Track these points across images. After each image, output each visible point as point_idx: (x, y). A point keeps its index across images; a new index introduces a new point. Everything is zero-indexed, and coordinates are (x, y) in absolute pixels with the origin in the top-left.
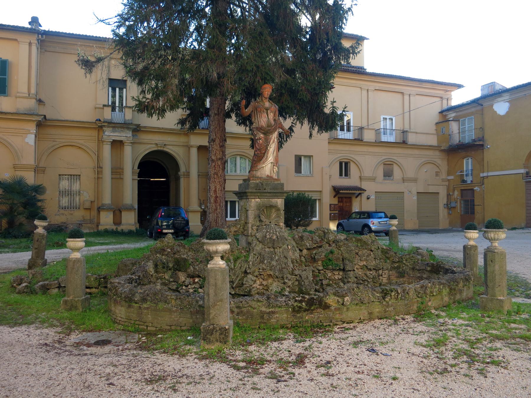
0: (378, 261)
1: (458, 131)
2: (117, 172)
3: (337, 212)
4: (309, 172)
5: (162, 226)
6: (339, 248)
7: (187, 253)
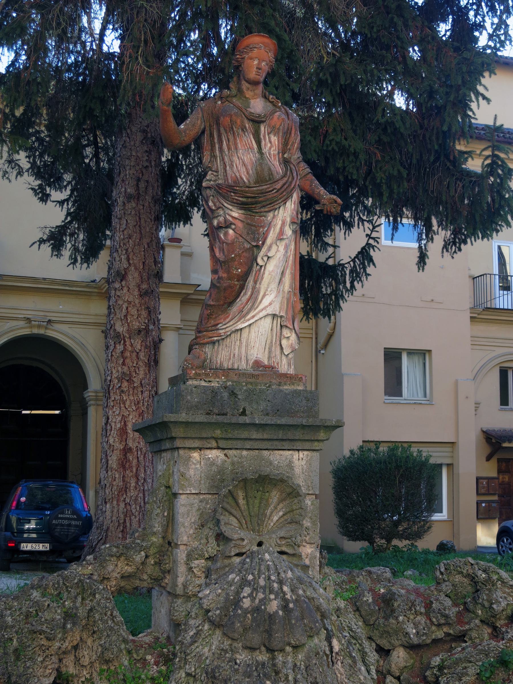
3: (496, 498)
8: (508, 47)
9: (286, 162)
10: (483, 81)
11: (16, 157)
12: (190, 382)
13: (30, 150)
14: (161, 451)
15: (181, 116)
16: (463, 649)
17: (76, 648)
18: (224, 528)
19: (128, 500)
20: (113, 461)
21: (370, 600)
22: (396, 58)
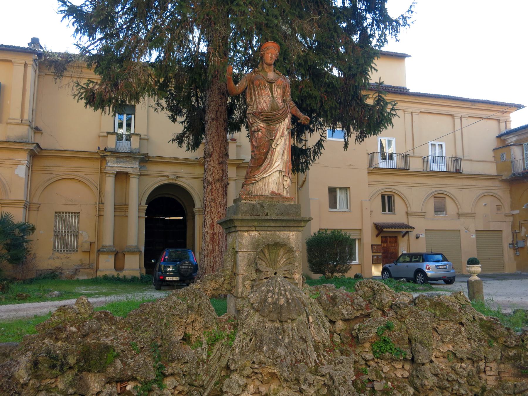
0: (475, 345)
1: (521, 157)
2: (121, 209)
3: (381, 254)
4: (345, 207)
5: (166, 272)
6: (401, 318)
7: (115, 332)
8: (386, 45)
9: (284, 101)
10: (374, 61)
11: (161, 101)
12: (243, 201)
13: (167, 98)
14: (230, 233)
15: (236, 82)
16: (369, 321)
17: (193, 322)
18: (259, 267)
19: (215, 256)
20: (208, 238)
21: (326, 299)
22: (334, 52)
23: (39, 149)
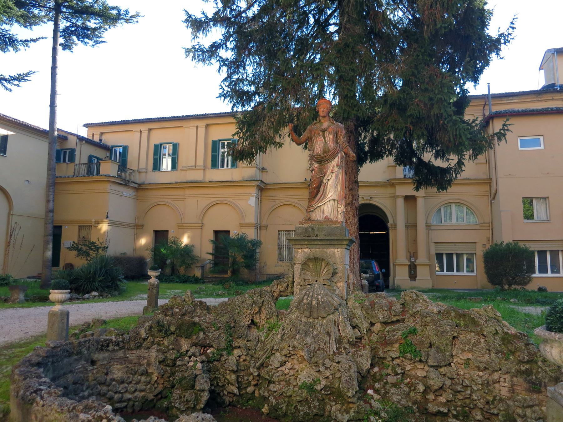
7: (205, 315)
23: (263, 184)
